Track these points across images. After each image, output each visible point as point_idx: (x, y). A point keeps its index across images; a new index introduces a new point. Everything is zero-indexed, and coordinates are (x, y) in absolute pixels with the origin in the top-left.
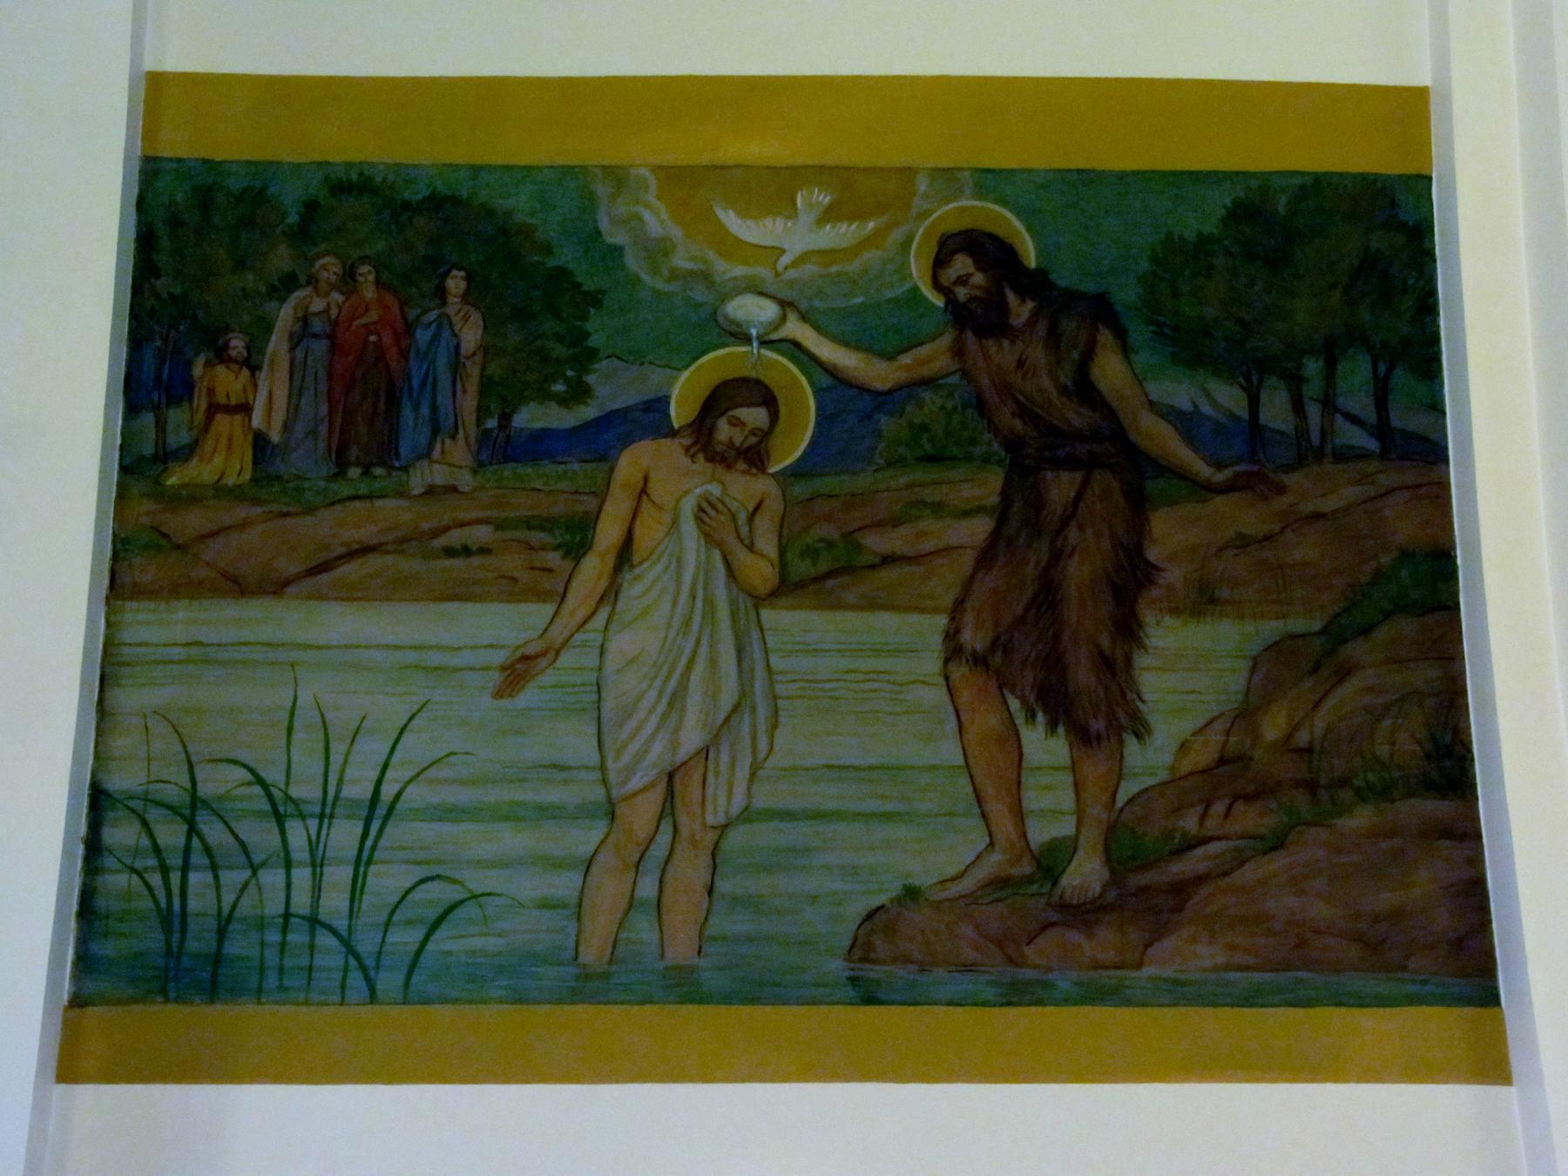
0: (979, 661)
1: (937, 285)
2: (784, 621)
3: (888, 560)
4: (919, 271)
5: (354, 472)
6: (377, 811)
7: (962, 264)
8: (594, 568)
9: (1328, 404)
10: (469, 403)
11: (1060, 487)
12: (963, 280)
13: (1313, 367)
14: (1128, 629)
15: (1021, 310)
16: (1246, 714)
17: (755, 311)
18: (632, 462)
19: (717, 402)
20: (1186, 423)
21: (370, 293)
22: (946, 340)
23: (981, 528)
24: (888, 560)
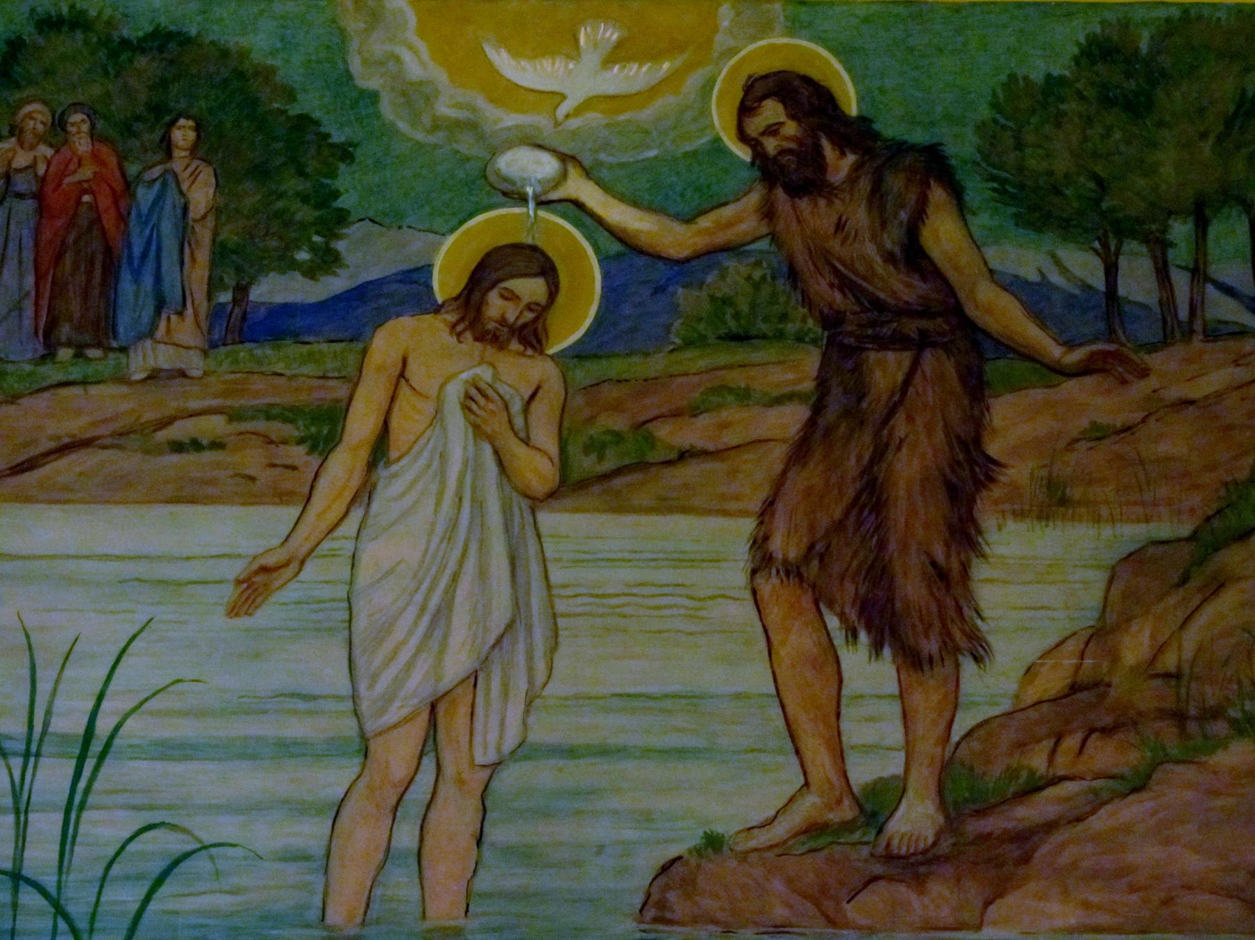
0: (792, 571)
1: (743, 137)
2: (564, 525)
3: (684, 455)
4: (721, 121)
5: (65, 354)
6: (91, 749)
7: (772, 111)
8: (343, 466)
9: (1198, 273)
10: (199, 274)
11: (886, 369)
12: (772, 130)
13: (1181, 230)
14: (965, 534)
15: (840, 165)
16: (1101, 635)
17: (531, 166)
18: (390, 340)
19: (487, 272)
20: (1034, 296)
21: (83, 145)
22: (754, 198)
23: (791, 419)
24: (684, 455)
